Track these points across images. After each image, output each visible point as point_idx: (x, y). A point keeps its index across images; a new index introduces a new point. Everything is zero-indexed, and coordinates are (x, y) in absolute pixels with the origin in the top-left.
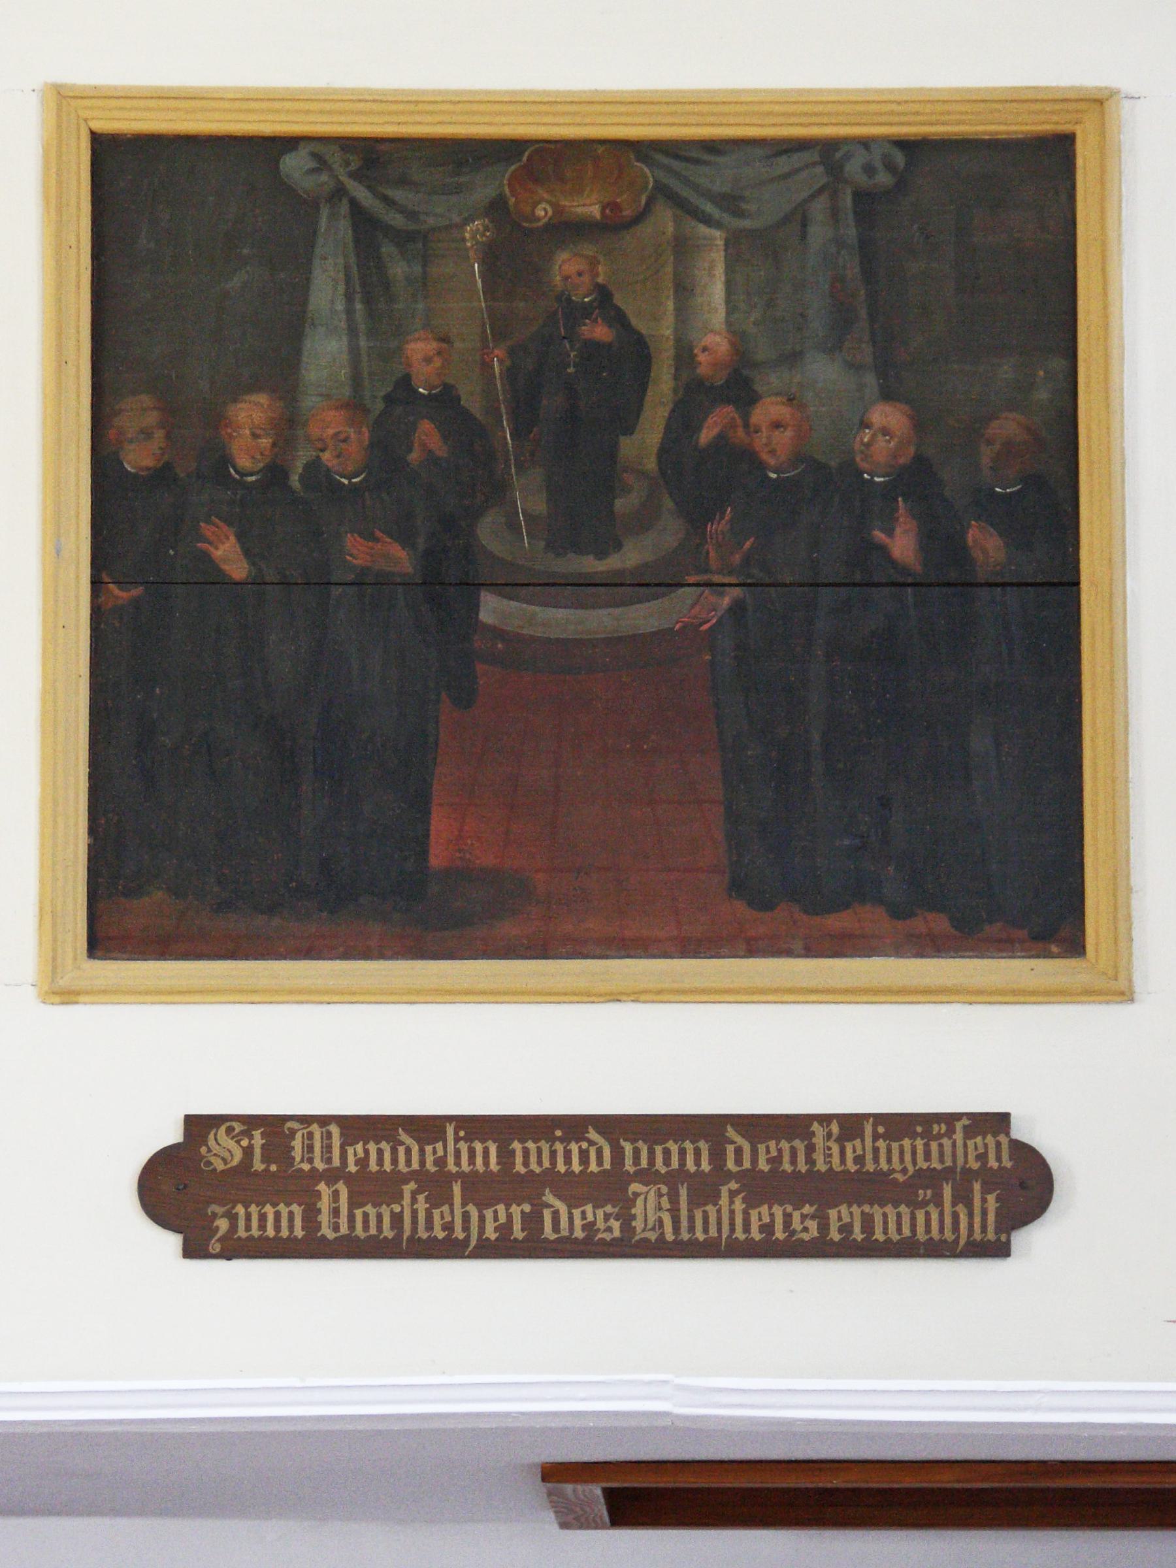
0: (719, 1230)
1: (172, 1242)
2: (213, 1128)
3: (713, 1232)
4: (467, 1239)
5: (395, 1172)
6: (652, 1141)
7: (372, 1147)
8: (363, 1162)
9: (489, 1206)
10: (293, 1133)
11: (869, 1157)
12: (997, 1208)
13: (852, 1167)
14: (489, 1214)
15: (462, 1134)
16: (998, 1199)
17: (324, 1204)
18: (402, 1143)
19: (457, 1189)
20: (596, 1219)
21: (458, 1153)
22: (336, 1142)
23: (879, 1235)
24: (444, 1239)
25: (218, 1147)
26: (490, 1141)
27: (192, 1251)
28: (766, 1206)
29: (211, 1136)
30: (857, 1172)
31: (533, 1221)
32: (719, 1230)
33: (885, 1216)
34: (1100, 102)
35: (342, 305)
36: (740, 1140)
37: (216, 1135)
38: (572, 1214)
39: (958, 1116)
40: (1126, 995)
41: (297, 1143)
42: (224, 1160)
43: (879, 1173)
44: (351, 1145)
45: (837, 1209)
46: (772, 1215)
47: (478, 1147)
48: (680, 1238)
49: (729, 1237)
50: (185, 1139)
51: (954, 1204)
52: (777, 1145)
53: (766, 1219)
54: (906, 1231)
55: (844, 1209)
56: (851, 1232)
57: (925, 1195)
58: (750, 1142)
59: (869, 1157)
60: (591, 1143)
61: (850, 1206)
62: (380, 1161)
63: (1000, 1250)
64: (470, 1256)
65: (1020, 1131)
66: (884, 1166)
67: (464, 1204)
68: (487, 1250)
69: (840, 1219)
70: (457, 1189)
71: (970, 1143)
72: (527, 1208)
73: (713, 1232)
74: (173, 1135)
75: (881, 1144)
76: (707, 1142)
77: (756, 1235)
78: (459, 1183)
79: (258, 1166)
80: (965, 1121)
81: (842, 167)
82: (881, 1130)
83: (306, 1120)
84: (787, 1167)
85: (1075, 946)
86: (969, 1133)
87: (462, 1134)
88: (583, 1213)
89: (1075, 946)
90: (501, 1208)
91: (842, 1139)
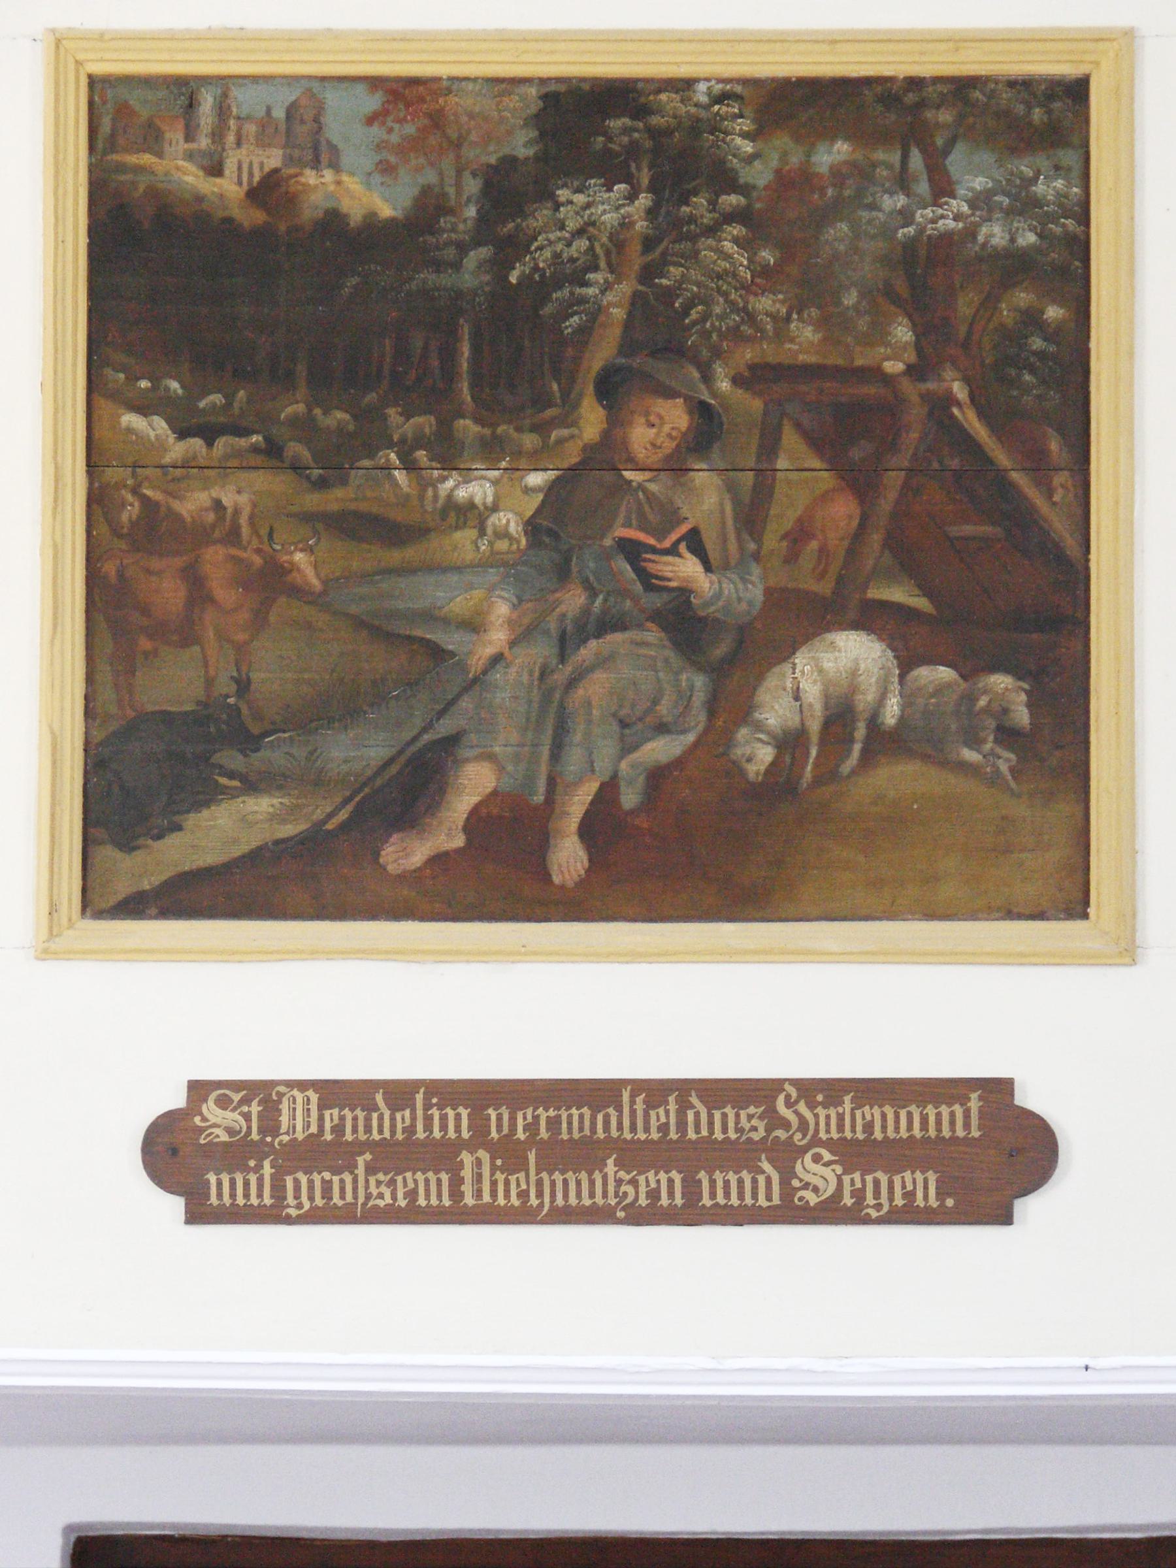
0: (356, 1197)
3: (349, 1197)
4: (541, 1205)
6: (739, 1105)
8: (338, 1130)
10: (281, 1095)
13: (860, 1136)
14: (897, 1180)
17: (467, 1173)
19: (532, 1157)
21: (428, 1120)
22: (314, 1107)
23: (469, 1200)
26: (461, 1107)
30: (864, 1140)
32: (356, 1197)
34: (58, 43)
35: (828, 232)
41: (284, 1107)
45: (516, 1176)
47: (451, 1113)
49: (364, 1204)
52: (534, 1111)
55: (908, 1175)
56: (659, 1198)
61: (913, 1173)
63: (1005, 1217)
64: (543, 1222)
68: (638, 1217)
70: (532, 1157)
71: (327, 1113)
73: (349, 1197)
74: (177, 1100)
77: (515, 1201)
78: (534, 1151)
79: (255, 1136)
81: (938, 123)
83: (291, 1084)
84: (878, 1135)
88: (852, 1181)
90: (857, 1176)
91: (650, 1105)
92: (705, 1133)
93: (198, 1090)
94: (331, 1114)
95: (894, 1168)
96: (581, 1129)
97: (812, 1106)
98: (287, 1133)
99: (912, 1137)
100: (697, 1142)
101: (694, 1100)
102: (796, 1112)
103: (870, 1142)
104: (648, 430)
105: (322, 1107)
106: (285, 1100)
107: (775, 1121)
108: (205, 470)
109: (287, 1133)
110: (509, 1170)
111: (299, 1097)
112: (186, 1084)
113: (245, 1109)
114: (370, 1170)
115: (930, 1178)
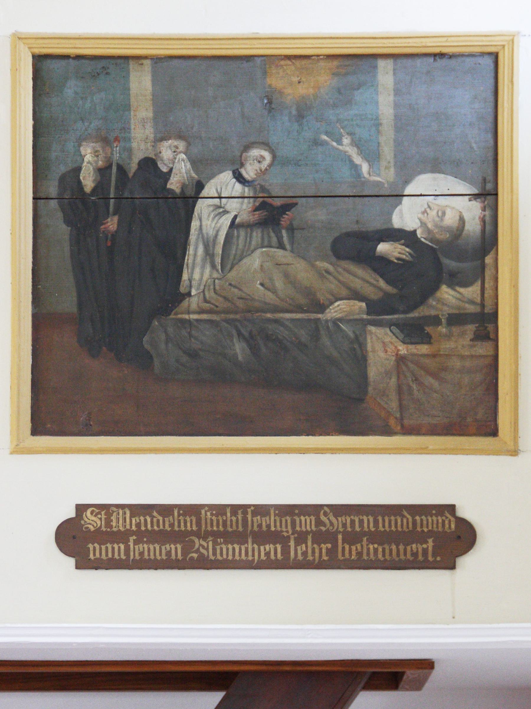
0: (253, 555)
1: (71, 562)
2: (84, 513)
5: (186, 530)
7: (142, 518)
9: (354, 544)
11: (176, 524)
12: (433, 546)
15: (277, 512)
16: (433, 541)
18: (405, 517)
19: (310, 537)
20: (144, 550)
24: (432, 561)
25: (89, 521)
27: (78, 567)
28: (141, 545)
29: (84, 515)
31: (332, 552)
33: (155, 548)
36: (409, 516)
37: (86, 514)
38: (101, 547)
39: (249, 506)
40: (515, 452)
42: (93, 526)
43: (276, 531)
44: (134, 517)
46: (144, 548)
47: (188, 519)
48: (228, 558)
50: (76, 516)
51: (343, 543)
53: (141, 550)
54: (110, 555)
57: (220, 541)
58: (411, 516)
59: (176, 524)
60: (447, 518)
62: (146, 525)
65: (461, 513)
66: (279, 529)
67: (313, 544)
69: (265, 550)
72: (329, 546)
74: (72, 514)
75: (181, 518)
76: (372, 516)
80: (252, 508)
82: (277, 512)
83: (118, 506)
84: (176, 528)
85: (36, 431)
86: (254, 514)
87: (181, 512)
89: (36, 431)
92: (161, 527)
93: (81, 509)
94: (257, 519)
95: (162, 543)
96: (408, 527)
97: (336, 516)
98: (115, 527)
99: (192, 530)
100: (232, 532)
101: (405, 513)
102: (329, 519)
103: (173, 531)
104: (478, 216)
105: (131, 517)
106: (115, 514)
107: (319, 523)
108: (196, 262)
109: (115, 527)
110: (351, 544)
111: (121, 512)
112: (75, 506)
113: (99, 516)
114: (136, 543)
115: (172, 547)
